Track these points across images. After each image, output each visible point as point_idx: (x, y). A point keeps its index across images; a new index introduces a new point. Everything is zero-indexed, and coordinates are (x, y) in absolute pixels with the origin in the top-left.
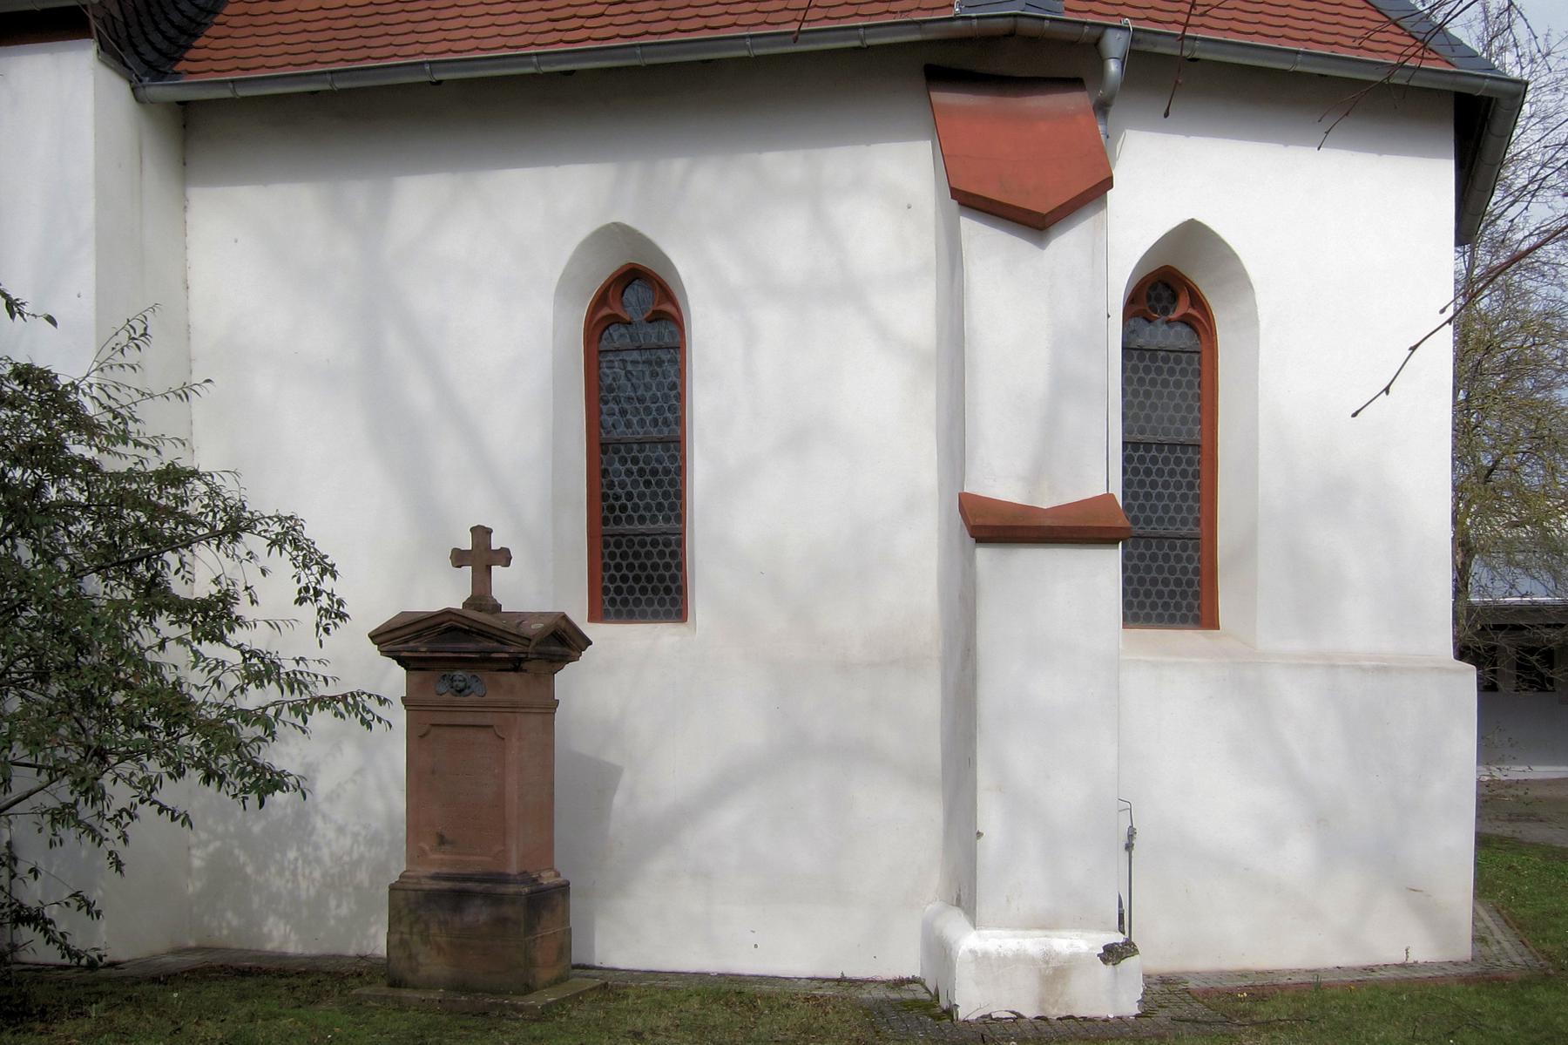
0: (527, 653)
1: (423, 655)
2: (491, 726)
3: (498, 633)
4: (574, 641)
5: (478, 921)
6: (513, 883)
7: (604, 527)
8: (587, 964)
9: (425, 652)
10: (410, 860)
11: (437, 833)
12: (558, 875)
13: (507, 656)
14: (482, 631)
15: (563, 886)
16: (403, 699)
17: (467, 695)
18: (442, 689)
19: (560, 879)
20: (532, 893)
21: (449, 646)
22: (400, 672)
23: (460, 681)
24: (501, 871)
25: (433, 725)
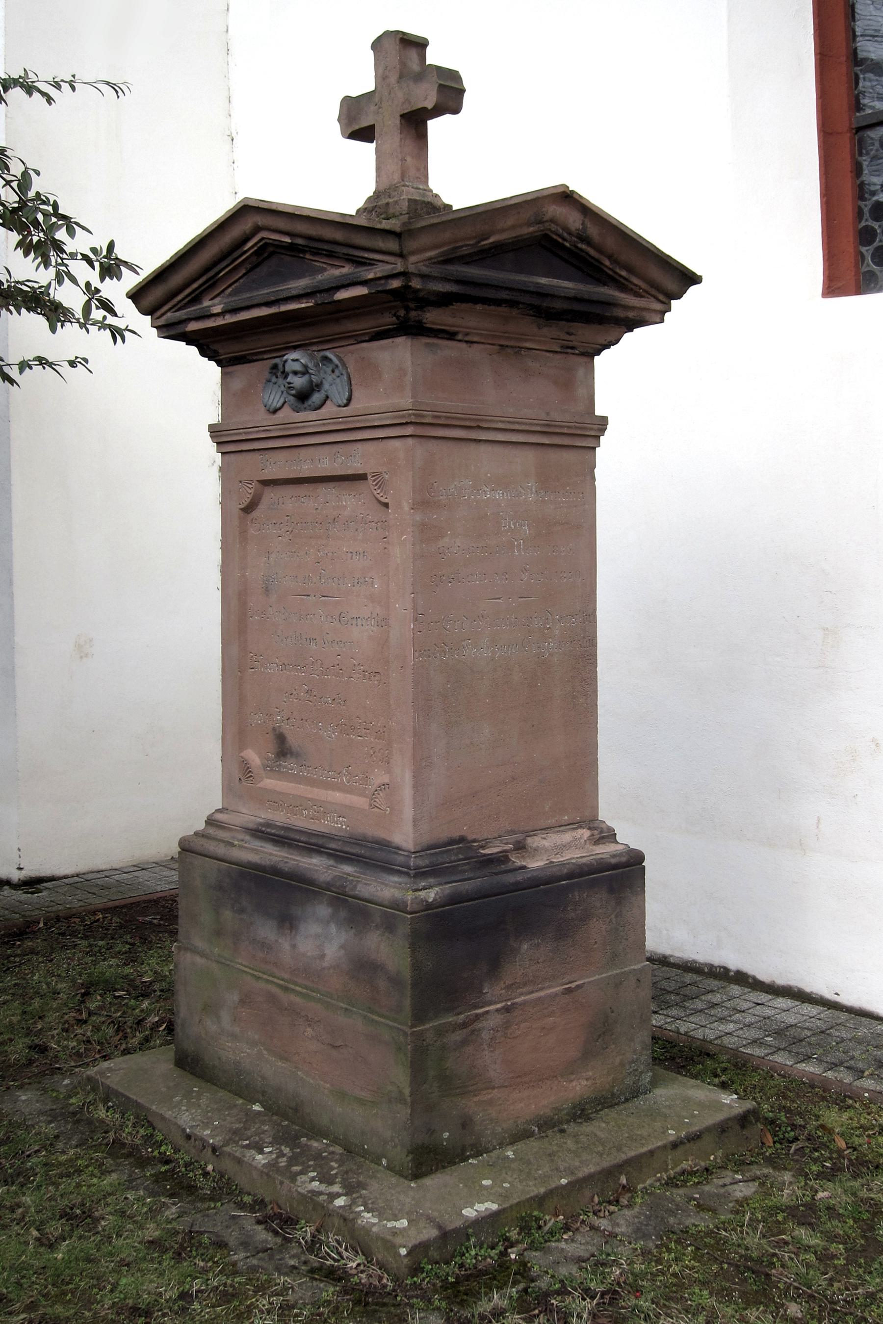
0: (404, 274)
1: (220, 322)
2: (362, 477)
3: (339, 236)
4: (630, 270)
5: (322, 956)
6: (399, 873)
7: (858, 114)
8: (808, 989)
9: (222, 314)
10: (228, 788)
11: (274, 729)
12: (610, 836)
13: (361, 291)
14: (320, 240)
15: (627, 865)
16: (215, 431)
17: (319, 407)
18: (275, 398)
19: (605, 850)
20: (454, 899)
21: (264, 293)
22: (212, 371)
23: (295, 373)
24: (381, 834)
25: (266, 483)
